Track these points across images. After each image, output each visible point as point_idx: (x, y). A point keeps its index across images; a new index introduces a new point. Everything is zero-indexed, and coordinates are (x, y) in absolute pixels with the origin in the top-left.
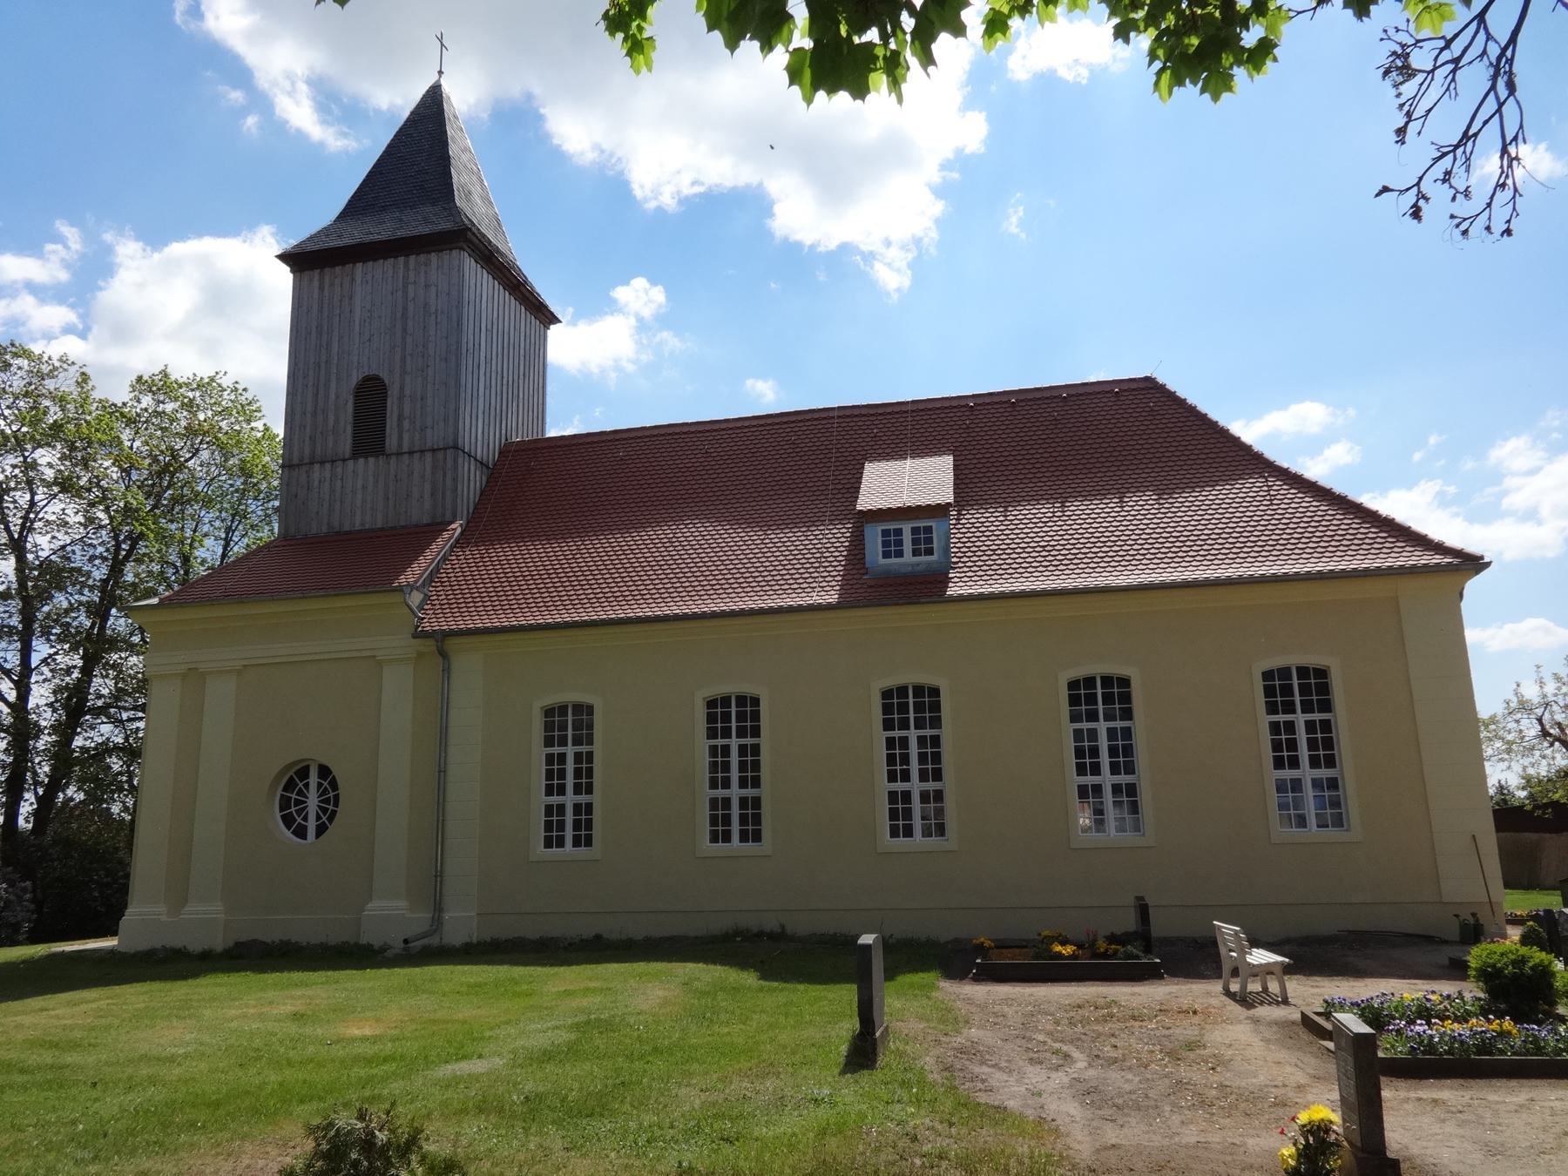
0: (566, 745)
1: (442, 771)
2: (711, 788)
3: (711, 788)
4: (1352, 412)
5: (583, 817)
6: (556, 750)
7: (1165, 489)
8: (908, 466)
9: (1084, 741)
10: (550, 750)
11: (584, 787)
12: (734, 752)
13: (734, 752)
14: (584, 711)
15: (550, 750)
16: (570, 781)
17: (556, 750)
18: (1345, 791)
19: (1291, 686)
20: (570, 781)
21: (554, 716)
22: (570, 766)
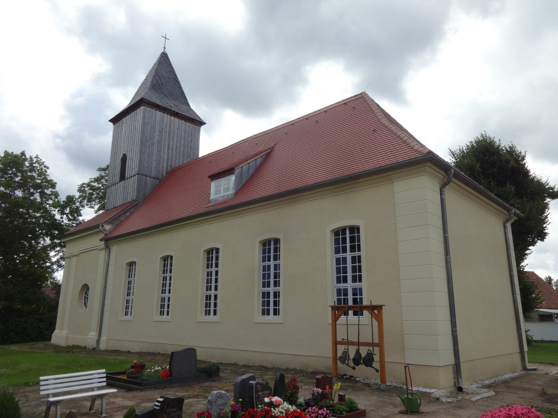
0: (346, 252)
1: (108, 263)
2: (337, 283)
3: (337, 283)
4: (22, 189)
5: (342, 297)
6: (341, 255)
7: (390, 115)
8: (38, 182)
9: (356, 266)
10: (338, 256)
11: (357, 279)
12: (349, 261)
13: (349, 261)
14: (355, 230)
15: (338, 256)
16: (349, 274)
17: (341, 255)
18: (266, 290)
19: (351, 242)
20: (349, 274)
21: (339, 233)
22: (349, 265)
